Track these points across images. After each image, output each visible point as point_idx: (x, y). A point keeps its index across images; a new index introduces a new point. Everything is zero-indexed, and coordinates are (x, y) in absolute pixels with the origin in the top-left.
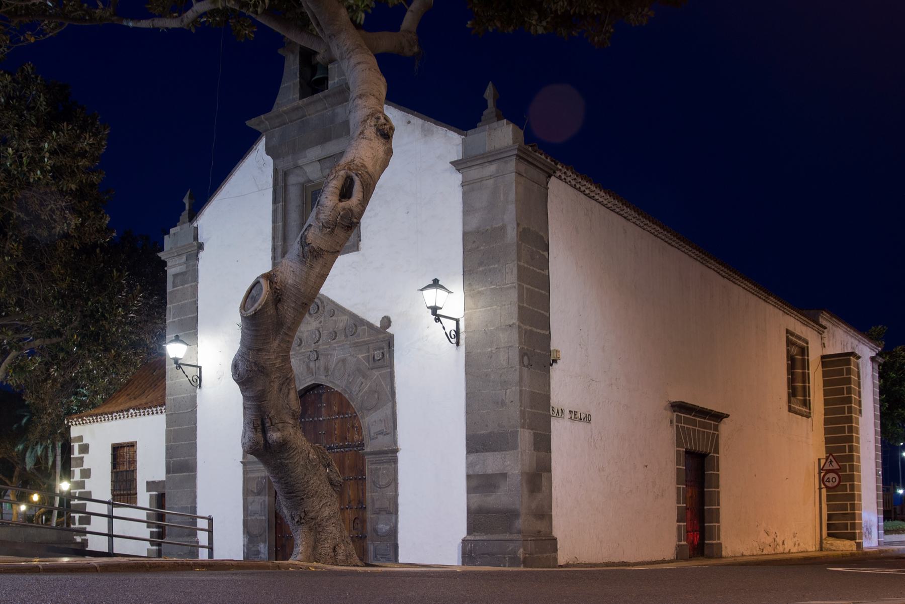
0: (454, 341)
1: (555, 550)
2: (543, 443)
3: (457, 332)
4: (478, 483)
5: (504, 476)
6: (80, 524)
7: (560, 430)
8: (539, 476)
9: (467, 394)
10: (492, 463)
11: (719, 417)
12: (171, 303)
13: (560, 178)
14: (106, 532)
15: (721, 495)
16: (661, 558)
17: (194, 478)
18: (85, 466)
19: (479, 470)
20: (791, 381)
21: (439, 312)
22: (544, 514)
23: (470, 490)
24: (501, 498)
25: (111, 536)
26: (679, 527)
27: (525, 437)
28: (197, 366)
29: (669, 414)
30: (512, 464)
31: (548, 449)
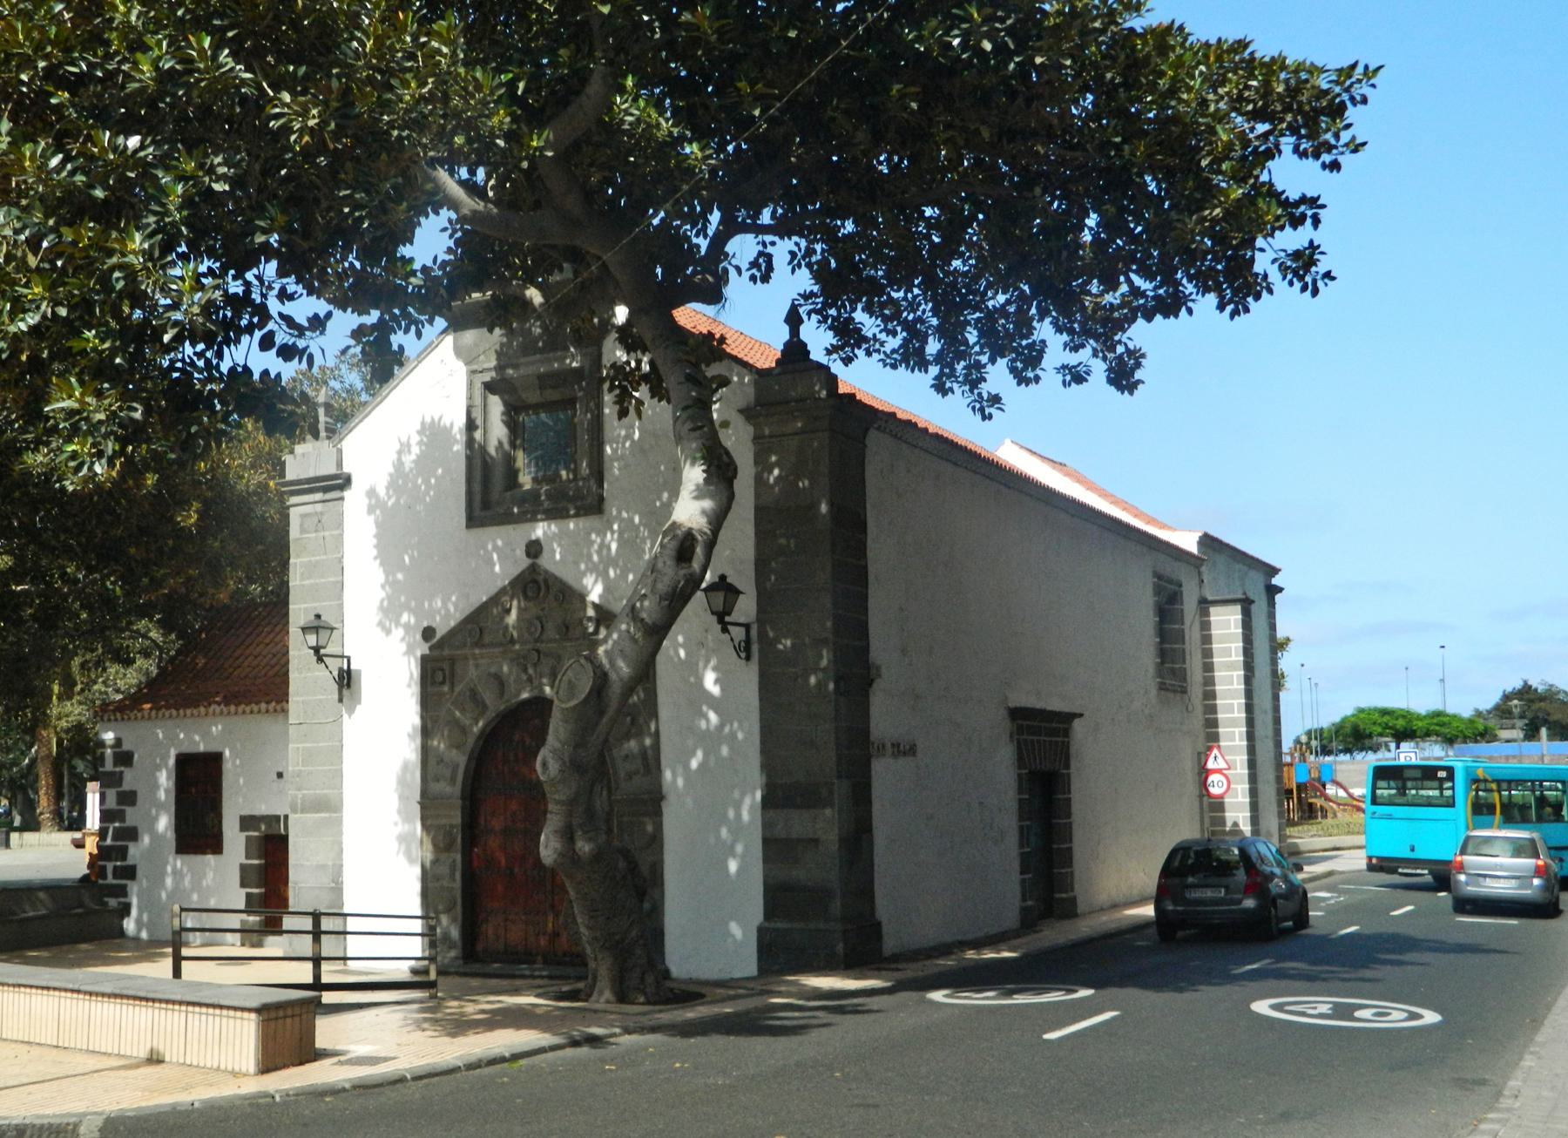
0: (743, 655)
1: (879, 937)
2: (861, 795)
3: (748, 641)
4: (775, 848)
5: (815, 842)
6: (115, 877)
7: (883, 772)
8: (858, 837)
9: (762, 727)
10: (799, 823)
11: (1070, 717)
12: (298, 556)
13: (878, 429)
14: (310, 954)
15: (1074, 827)
16: (882, 646)
17: (339, 822)
18: (126, 787)
19: (779, 831)
20: (1163, 654)
21: (727, 619)
22: (864, 892)
23: (767, 859)
24: (807, 872)
25: (317, 961)
26: (1023, 882)
27: (842, 789)
28: (342, 657)
29: (1006, 725)
30: (825, 825)
31: (868, 801)
